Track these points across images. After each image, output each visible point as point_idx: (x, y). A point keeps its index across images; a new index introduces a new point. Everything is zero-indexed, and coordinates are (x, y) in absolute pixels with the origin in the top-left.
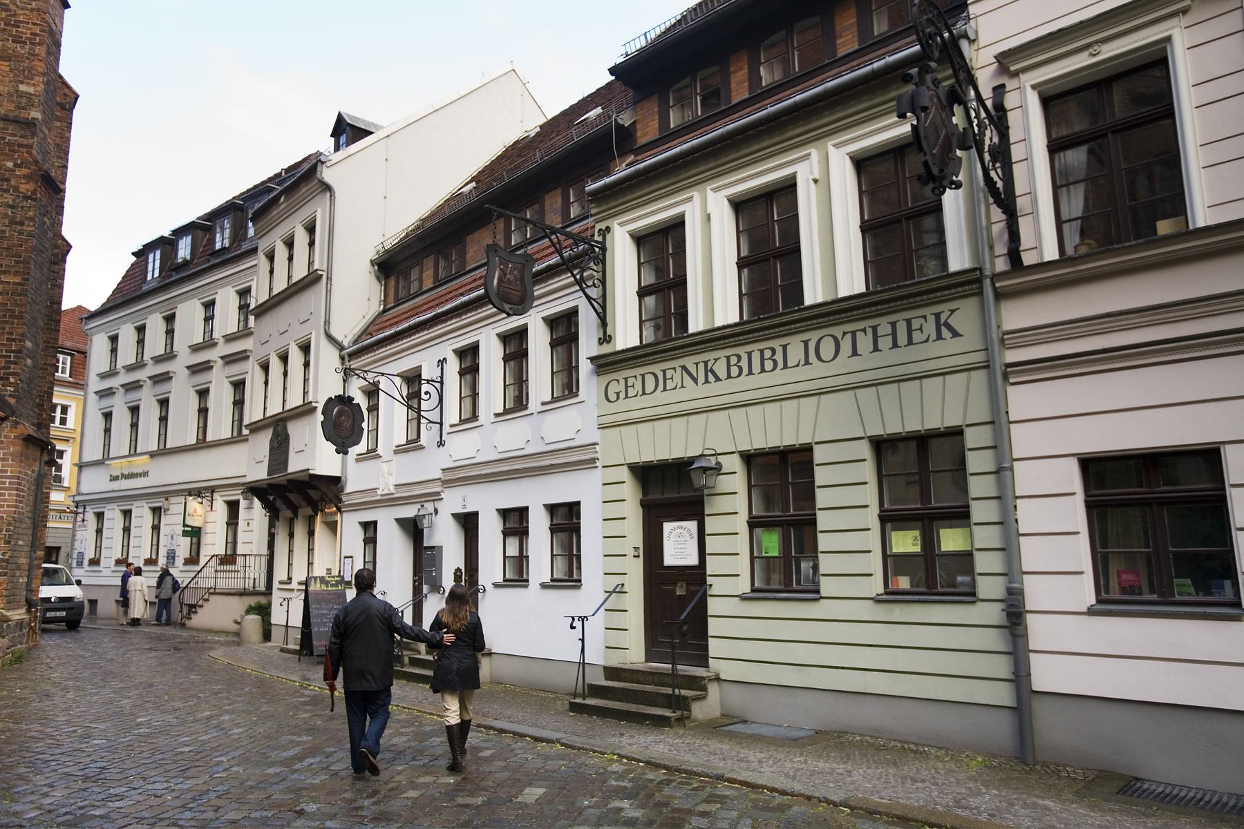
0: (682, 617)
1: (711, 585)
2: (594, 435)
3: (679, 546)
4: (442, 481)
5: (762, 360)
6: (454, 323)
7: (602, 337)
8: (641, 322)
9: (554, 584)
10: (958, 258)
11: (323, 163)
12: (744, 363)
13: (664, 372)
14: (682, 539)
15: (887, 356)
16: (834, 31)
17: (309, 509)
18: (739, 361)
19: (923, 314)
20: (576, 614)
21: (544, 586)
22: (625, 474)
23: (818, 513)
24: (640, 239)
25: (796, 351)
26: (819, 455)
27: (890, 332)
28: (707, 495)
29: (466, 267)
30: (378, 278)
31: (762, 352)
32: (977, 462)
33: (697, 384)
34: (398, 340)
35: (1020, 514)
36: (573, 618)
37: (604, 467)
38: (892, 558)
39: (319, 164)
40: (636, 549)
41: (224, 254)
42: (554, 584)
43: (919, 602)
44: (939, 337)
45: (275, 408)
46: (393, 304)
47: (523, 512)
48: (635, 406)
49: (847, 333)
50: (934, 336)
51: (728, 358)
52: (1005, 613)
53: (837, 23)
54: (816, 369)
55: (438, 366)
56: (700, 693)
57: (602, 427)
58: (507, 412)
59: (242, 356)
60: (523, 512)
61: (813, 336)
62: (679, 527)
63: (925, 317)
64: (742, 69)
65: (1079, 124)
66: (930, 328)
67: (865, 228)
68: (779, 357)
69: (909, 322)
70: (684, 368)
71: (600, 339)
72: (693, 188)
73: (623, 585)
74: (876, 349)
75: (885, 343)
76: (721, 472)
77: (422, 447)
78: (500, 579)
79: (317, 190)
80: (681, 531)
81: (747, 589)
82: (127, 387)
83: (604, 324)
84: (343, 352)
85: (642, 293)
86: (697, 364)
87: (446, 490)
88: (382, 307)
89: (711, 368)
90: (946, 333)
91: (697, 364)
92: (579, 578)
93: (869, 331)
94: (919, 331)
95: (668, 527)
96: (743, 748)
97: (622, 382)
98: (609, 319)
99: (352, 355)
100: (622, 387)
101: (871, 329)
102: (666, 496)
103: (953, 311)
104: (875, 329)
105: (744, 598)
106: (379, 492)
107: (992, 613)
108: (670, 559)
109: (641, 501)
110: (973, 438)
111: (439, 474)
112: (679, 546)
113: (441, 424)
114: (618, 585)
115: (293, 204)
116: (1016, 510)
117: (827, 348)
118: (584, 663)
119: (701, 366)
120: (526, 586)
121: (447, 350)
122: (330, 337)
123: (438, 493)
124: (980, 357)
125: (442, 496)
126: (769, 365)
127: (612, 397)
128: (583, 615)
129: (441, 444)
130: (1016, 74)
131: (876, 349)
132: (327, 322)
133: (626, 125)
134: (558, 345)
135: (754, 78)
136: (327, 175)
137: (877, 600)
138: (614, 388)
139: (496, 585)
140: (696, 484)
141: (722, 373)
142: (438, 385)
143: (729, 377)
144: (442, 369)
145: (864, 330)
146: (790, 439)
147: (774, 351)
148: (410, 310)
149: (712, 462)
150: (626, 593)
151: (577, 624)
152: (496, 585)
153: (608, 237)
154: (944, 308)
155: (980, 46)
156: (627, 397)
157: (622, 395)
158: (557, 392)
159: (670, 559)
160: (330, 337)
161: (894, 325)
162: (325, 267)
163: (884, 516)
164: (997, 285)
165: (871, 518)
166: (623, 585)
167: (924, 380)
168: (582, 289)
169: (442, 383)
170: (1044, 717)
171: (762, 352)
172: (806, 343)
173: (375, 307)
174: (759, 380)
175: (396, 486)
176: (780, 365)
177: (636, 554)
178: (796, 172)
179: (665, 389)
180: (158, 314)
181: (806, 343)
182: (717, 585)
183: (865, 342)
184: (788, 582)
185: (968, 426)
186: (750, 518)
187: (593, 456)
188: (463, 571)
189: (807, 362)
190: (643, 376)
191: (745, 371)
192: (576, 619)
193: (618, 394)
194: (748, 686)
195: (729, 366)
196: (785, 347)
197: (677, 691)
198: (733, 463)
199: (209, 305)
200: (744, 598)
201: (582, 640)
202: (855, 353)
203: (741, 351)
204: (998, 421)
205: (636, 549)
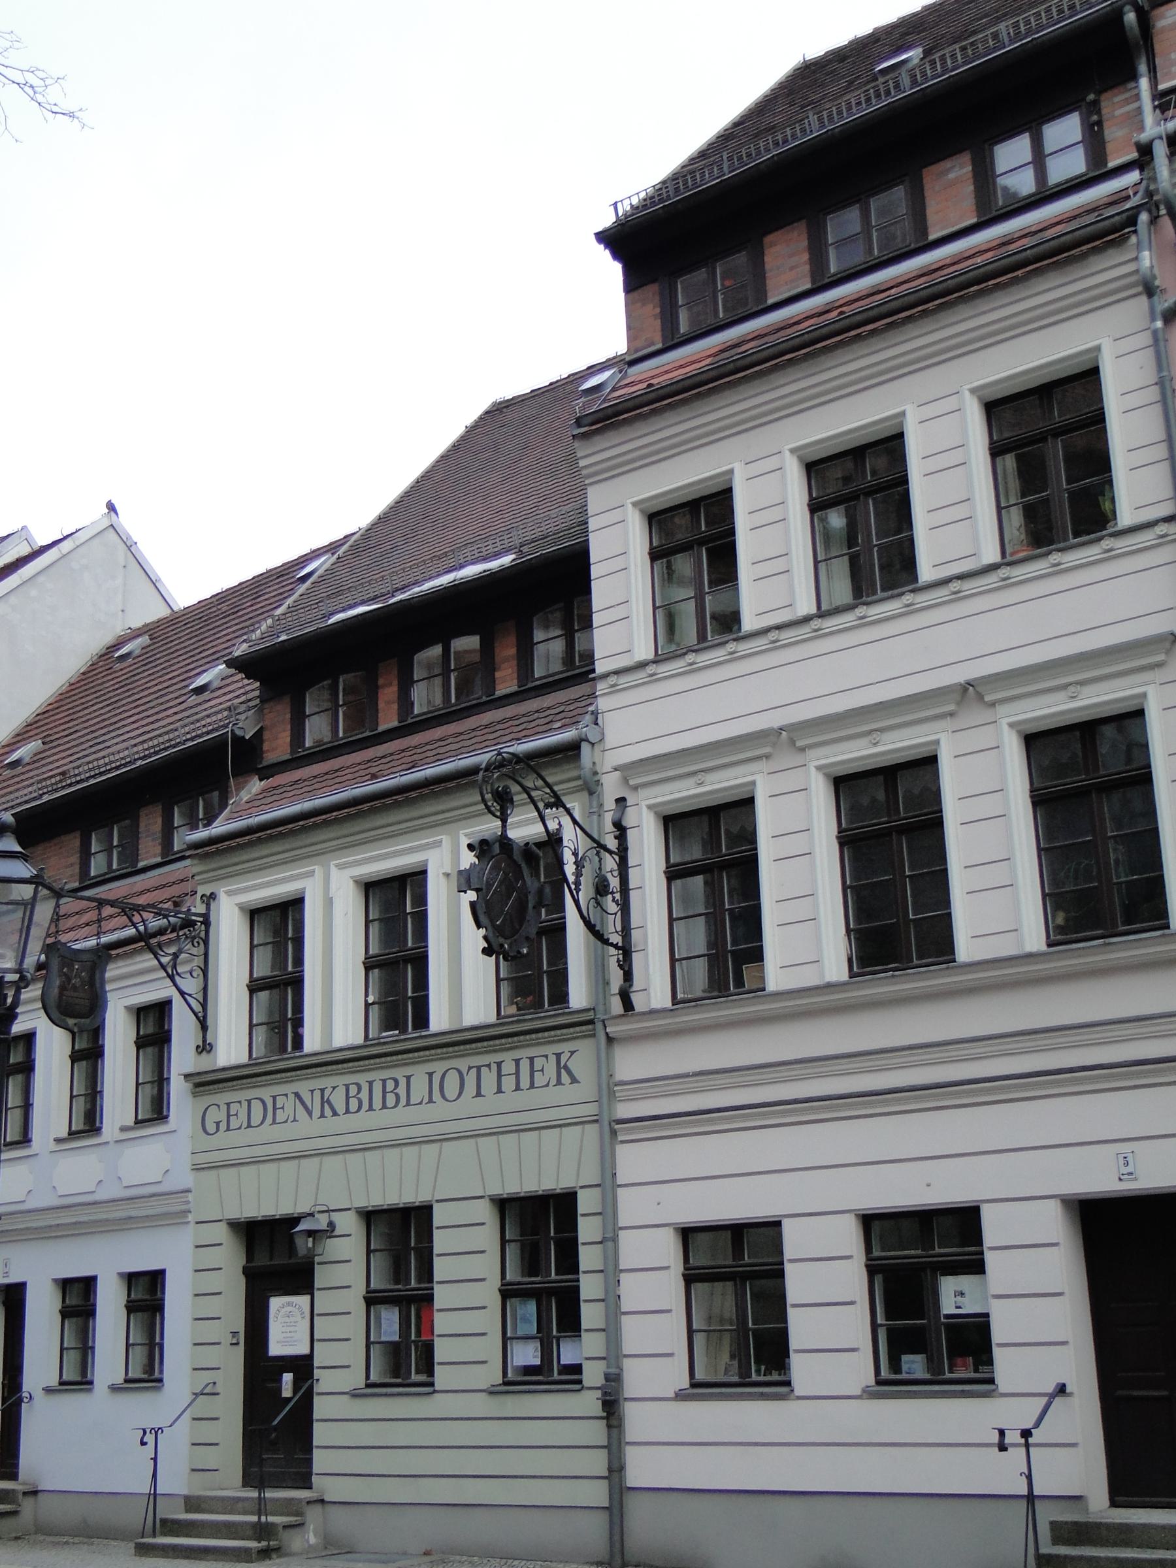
0: (275, 1422)
1: (318, 1380)
5: (384, 1092)
7: (201, 1044)
8: (251, 1026)
9: (131, 1383)
10: (579, 995)
13: (274, 1098)
14: (292, 1319)
16: (493, 663)
18: (359, 1092)
20: (148, 1425)
21: (114, 1389)
22: (221, 1233)
23: (436, 1287)
24: (254, 914)
26: (440, 1216)
27: (514, 1072)
28: (318, 1264)
32: (587, 1230)
33: (311, 1119)
35: (624, 1290)
36: (145, 1433)
37: (197, 1223)
40: (235, 1334)
42: (131, 1383)
47: (88, 1284)
48: (237, 1142)
49: (473, 1067)
50: (553, 1081)
51: (347, 1087)
52: (600, 1401)
53: (497, 651)
56: (295, 1518)
57: (198, 1168)
58: (73, 1135)
60: (88, 1284)
61: (438, 1067)
62: (289, 1304)
64: (390, 684)
65: (695, 852)
68: (402, 1090)
70: (297, 1095)
71: (198, 1047)
72: (314, 859)
73: (215, 1383)
74: (500, 1091)
75: (508, 1083)
76: (334, 1234)
78: (54, 1381)
80: (290, 1309)
81: (361, 1382)
83: (204, 1027)
85: (255, 987)
86: (312, 1091)
90: (565, 1077)
91: (312, 1091)
92: (160, 1376)
93: (494, 1067)
97: (224, 1108)
98: (209, 1022)
101: (495, 1065)
103: (572, 1053)
104: (499, 1064)
105: (355, 1395)
107: (588, 1402)
108: (276, 1348)
109: (244, 1268)
110: (586, 1202)
114: (207, 1385)
116: (619, 1285)
118: (155, 1494)
119: (317, 1094)
120: (90, 1390)
127: (211, 1127)
128: (156, 1426)
130: (635, 788)
131: (500, 1091)
133: (247, 737)
135: (405, 703)
137: (492, 1392)
138: (214, 1115)
139: (48, 1391)
140: (302, 1252)
141: (340, 1107)
143: (347, 1111)
145: (489, 1066)
147: (359, 1088)
149: (322, 1222)
151: (150, 1438)
152: (48, 1391)
153: (213, 906)
155: (606, 748)
156: (228, 1129)
157: (223, 1126)
158: (143, 1111)
159: (276, 1348)
161: (517, 1062)
166: (215, 1383)
168: (171, 978)
172: (431, 1075)
174: (380, 1118)
176: (403, 1101)
177: (234, 1341)
179: (274, 1122)
181: (431, 1075)
182: (324, 1381)
183: (489, 1078)
186: (368, 1292)
187: (184, 1207)
189: (431, 1101)
190: (249, 1101)
191: (365, 1106)
192: (148, 1431)
193: (218, 1124)
196: (408, 1078)
198: (349, 1224)
200: (355, 1395)
201: (155, 1459)
202: (479, 1094)
203: (362, 1079)
204: (608, 1184)
205: (235, 1334)
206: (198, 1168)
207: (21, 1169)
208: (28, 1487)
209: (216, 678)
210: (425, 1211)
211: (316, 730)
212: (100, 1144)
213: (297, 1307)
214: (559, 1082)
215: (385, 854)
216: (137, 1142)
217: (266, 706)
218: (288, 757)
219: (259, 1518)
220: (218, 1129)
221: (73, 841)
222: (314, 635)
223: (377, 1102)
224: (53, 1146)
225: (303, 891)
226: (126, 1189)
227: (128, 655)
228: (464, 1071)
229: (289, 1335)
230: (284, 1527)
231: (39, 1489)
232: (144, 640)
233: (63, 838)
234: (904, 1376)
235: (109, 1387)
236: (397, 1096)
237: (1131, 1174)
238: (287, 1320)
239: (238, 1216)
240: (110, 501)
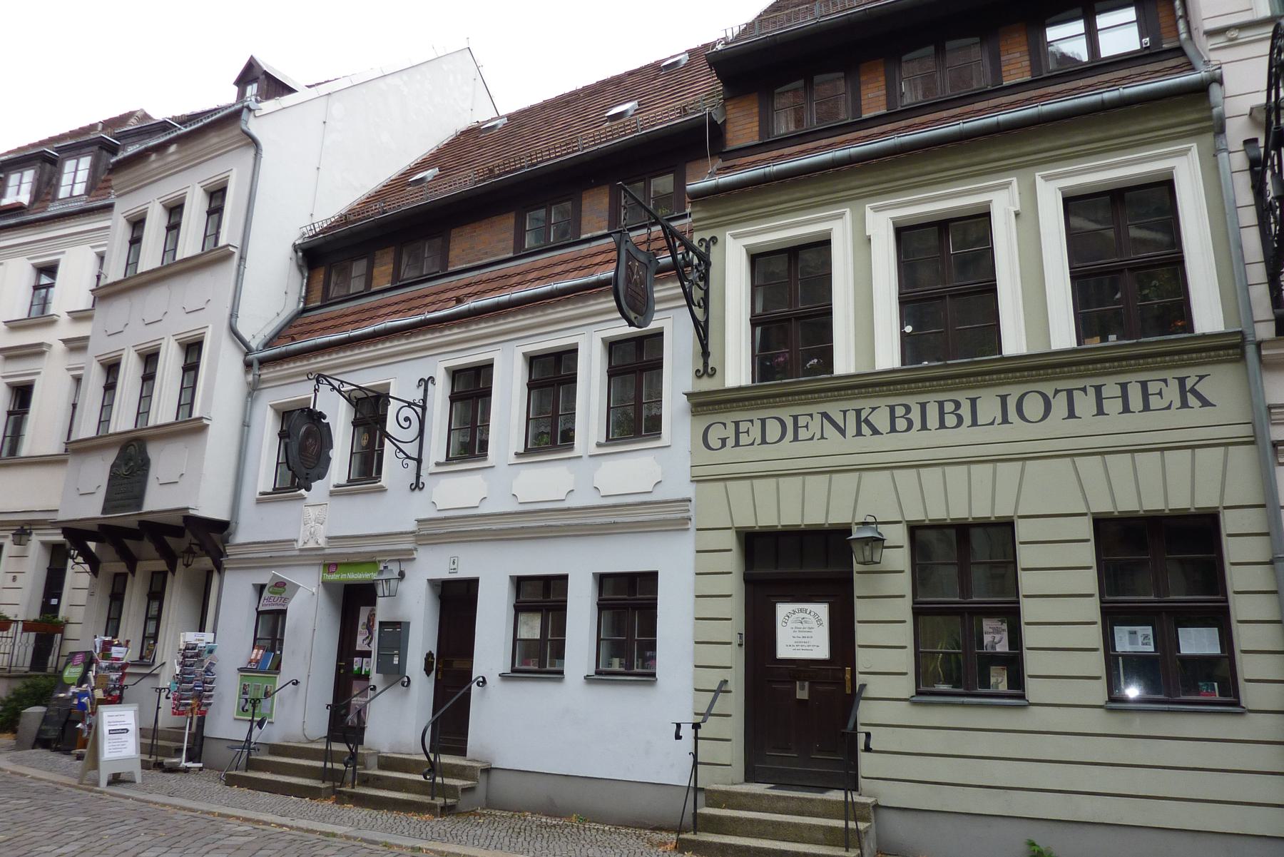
2: (689, 491)
3: (801, 635)
4: (416, 536)
6: (455, 333)
11: (250, 110)
12: (915, 415)
13: (795, 418)
15: (1115, 418)
17: (163, 562)
19: (751, 419)
25: (989, 405)
26: (1023, 531)
29: (447, 267)
30: (300, 268)
31: (941, 404)
33: (845, 438)
34: (352, 348)
38: (605, 642)
39: (245, 111)
41: (22, 214)
43: (1169, 711)
44: (1184, 404)
45: (123, 421)
46: (319, 304)
47: (470, 586)
48: (750, 456)
49: (1062, 390)
51: (892, 409)
53: (863, 93)
54: (1017, 428)
55: (419, 386)
59: (36, 351)
60: (470, 586)
61: (1014, 392)
62: (801, 610)
63: (811, 415)
66: (1172, 393)
67: (755, 322)
68: (965, 411)
69: (1144, 385)
70: (825, 415)
71: (698, 371)
75: (1113, 406)
77: (382, 490)
79: (235, 143)
82: (75, 315)
83: (705, 354)
84: (250, 357)
86: (845, 412)
87: (421, 549)
88: (301, 305)
89: (866, 418)
90: (1192, 400)
91: (845, 412)
93: (1091, 391)
94: (1159, 396)
95: (783, 610)
96: (322, 801)
97: (731, 427)
99: (263, 362)
102: (829, 570)
103: (1201, 377)
104: (1098, 389)
106: (300, 545)
111: (412, 526)
112: (801, 635)
113: (419, 461)
115: (199, 154)
117: (1033, 406)
119: (851, 417)
121: (438, 368)
122: (233, 331)
123: (410, 551)
124: (1245, 431)
125: (415, 556)
126: (951, 420)
127: (714, 441)
129: (417, 486)
132: (233, 315)
134: (536, 388)
136: (253, 126)
142: (419, 410)
144: (426, 390)
145: (1084, 390)
146: (1180, 501)
147: (908, 409)
148: (353, 313)
150: (730, 692)
153: (713, 249)
154: (1191, 374)
160: (233, 331)
161: (1124, 386)
162: (238, 243)
163: (917, 608)
164: (1264, 353)
165: (1092, 610)
167: (1166, 453)
169: (424, 408)
171: (941, 404)
172: (1004, 399)
173: (291, 305)
174: (935, 436)
175: (330, 538)
178: (991, 201)
179: (796, 439)
180: (87, 247)
181: (1004, 399)
184: (542, 663)
185: (1225, 508)
187: (685, 515)
188: (435, 657)
189: (1005, 420)
190: (763, 421)
193: (724, 441)
194: (927, 815)
196: (973, 402)
197: (329, 765)
198: (897, 535)
199: (49, 270)
202: (1072, 414)
203: (913, 401)
207: (476, 479)
208: (484, 765)
209: (631, 108)
210: (1007, 526)
211: (784, 126)
212: (569, 458)
213: (812, 614)
216: (634, 453)
217: (727, 104)
218: (756, 142)
220: (724, 445)
221: (509, 221)
222: (619, 146)
224: (513, 460)
225: (829, 233)
226: (603, 498)
227: (422, 179)
228: (1051, 396)
230: (481, 770)
231: (493, 766)
232: (505, 120)
233: (494, 219)
234: (991, 691)
235: (500, 675)
238: (800, 625)
239: (775, 523)
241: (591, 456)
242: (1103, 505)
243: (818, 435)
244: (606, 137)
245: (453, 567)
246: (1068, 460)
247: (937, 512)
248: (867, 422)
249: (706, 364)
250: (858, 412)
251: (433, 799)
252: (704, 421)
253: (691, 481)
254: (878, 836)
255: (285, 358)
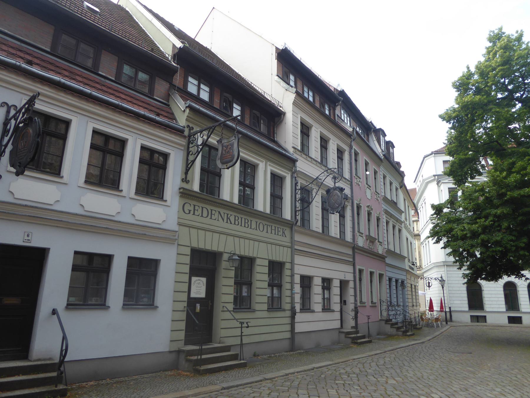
2: (175, 228)
5: (245, 222)
14: (200, 285)
32: (287, 272)
62: (199, 280)
68: (249, 223)
70: (219, 212)
80: (199, 282)
83: (186, 173)
91: (224, 213)
97: (193, 206)
100: (192, 208)
107: (288, 313)
110: (288, 266)
124: (290, 245)
138: (187, 207)
145: (269, 226)
170: (297, 338)
181: (257, 222)
189: (256, 229)
193: (190, 211)
195: (235, 220)
204: (292, 263)
206: (180, 224)
212: (118, 196)
214: (283, 236)
215: (257, 158)
219: (201, 357)
220: (189, 213)
223: (243, 225)
229: (198, 290)
236: (238, 222)
237: (29, 240)
238: (198, 285)
240: (440, 116)
241: (130, 198)
242: (195, 245)
243: (217, 219)
244: (122, 34)
245: (26, 238)
246: (188, 228)
247: (202, 246)
248: (284, 232)
249: (186, 177)
250: (228, 214)
251: (56, 387)
252: (184, 201)
253: (178, 224)
254: (290, 351)
255: (9, 67)
